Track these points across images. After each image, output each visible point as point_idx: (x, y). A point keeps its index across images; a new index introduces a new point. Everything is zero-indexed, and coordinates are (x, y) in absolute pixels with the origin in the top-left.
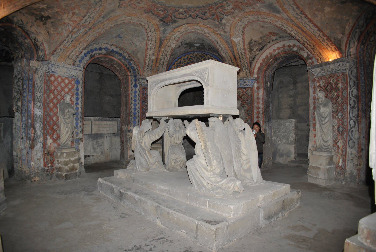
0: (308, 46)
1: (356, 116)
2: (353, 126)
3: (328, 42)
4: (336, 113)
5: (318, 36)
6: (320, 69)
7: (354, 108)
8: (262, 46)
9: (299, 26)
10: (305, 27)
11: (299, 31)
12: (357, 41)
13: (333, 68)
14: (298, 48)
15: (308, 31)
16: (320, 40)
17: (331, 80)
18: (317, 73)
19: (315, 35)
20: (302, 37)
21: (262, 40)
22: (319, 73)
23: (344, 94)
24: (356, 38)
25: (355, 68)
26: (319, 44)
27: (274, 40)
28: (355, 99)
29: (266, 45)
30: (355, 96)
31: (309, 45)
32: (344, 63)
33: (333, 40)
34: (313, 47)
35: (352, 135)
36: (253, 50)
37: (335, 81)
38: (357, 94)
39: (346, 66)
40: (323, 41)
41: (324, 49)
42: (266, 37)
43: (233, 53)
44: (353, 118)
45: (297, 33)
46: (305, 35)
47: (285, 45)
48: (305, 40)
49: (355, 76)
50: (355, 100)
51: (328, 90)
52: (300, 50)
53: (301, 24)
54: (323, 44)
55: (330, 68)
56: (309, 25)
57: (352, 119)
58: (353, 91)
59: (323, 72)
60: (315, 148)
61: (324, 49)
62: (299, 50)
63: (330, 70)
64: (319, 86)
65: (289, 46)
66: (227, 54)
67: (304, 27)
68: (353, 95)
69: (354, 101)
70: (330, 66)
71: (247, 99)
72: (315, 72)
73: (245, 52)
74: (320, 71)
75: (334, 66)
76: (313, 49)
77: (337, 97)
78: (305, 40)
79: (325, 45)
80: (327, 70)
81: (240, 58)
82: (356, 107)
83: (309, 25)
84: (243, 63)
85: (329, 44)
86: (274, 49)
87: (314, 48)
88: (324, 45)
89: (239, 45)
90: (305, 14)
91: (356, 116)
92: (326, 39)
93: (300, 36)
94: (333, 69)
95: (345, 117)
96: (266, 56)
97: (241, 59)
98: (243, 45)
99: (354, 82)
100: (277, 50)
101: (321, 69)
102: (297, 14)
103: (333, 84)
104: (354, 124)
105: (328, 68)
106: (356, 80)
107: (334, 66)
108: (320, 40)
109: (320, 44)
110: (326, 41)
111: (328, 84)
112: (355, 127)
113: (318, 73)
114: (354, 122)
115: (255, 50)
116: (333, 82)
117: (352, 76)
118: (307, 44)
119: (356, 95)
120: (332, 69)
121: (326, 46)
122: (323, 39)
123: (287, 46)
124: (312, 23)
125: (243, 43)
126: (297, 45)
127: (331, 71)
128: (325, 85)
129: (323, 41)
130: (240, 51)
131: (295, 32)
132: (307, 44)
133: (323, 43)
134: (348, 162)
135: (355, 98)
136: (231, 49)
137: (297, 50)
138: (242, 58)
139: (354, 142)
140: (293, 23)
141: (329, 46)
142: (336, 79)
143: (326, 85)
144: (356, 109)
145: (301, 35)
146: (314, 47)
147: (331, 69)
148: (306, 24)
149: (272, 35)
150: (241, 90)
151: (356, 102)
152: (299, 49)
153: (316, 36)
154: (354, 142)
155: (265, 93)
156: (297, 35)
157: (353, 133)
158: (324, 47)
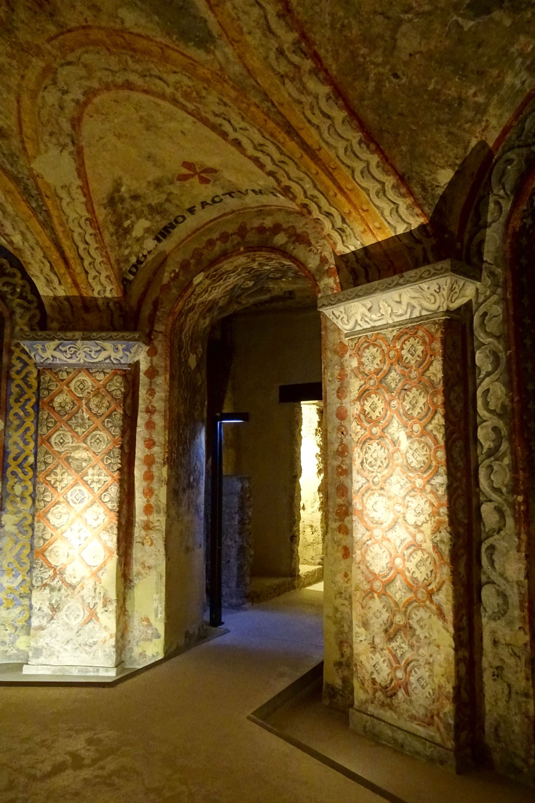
0: (321, 217)
1: (504, 490)
2: (496, 526)
3: (400, 202)
4: (425, 476)
5: (362, 172)
6: (364, 305)
7: (499, 454)
8: (165, 223)
9: (290, 126)
10: (313, 125)
11: (292, 146)
12: (512, 198)
13: (413, 302)
14: (290, 237)
15: (323, 145)
16: (366, 190)
17: (402, 349)
18: (352, 323)
19: (349, 167)
20: (302, 175)
21: (164, 197)
22: (359, 322)
23: (454, 403)
24: (508, 187)
25: (496, 303)
26: (365, 208)
27: (207, 204)
28: (501, 423)
29: (180, 219)
30: (498, 411)
31: (328, 215)
32: (456, 281)
33: (417, 190)
34: (339, 223)
35: (492, 563)
36: (128, 231)
37: (419, 352)
38: (507, 402)
39: (464, 296)
40: (381, 194)
41: (379, 228)
42: (178, 183)
43: (53, 236)
44: (494, 496)
45: (283, 158)
46: (314, 168)
47: (248, 227)
48: (312, 192)
49: (498, 334)
50: (500, 424)
51: (393, 386)
52: (297, 244)
53: (297, 108)
54: (378, 207)
55: (400, 302)
56: (329, 117)
57: (490, 501)
58: (488, 390)
59: (374, 317)
60: (346, 599)
61: (379, 228)
62: (294, 242)
63: (400, 312)
64: (358, 368)
65: (261, 230)
66: (29, 236)
67: (308, 125)
68: (492, 408)
69: (495, 429)
70: (400, 296)
71: (107, 412)
72: (345, 320)
73: (95, 235)
74: (363, 315)
75: (417, 295)
76: (341, 231)
77: (426, 415)
78: (312, 192)
79: (387, 213)
80: (389, 309)
81: (82, 259)
82: (504, 455)
83: (329, 117)
84: (94, 278)
85: (402, 210)
86: (209, 237)
87: (345, 226)
88: (382, 214)
89: (68, 199)
90: (316, 57)
91: (504, 490)
92: (393, 187)
93: (294, 172)
94: (414, 307)
95: (459, 491)
96: (184, 260)
97: (86, 263)
98: (86, 204)
99: (495, 354)
100: (219, 243)
101: (369, 306)
102: (281, 52)
103: (413, 362)
104: (499, 522)
105: (393, 304)
106: (501, 347)
107: (417, 295)
108: (366, 190)
109: (367, 211)
110: (391, 194)
111: (392, 364)
112: (502, 533)
113: (356, 321)
114: (499, 510)
115: (138, 232)
116: (413, 356)
117: (486, 332)
118: (319, 207)
119: (503, 406)
120: (408, 304)
121: (390, 219)
122: (379, 186)
123: (252, 229)
124: (341, 108)
125: (85, 195)
126: (285, 226)
127: (406, 312)
128: (381, 366)
129: (381, 194)
130: (77, 230)
131: (277, 156)
132: (319, 207)
133: (377, 202)
134: (314, 404)
135: (500, 416)
136: (41, 218)
137: (287, 243)
138: (90, 260)
139: (502, 595)
140: (266, 105)
141: (400, 217)
142: (424, 343)
143: (386, 368)
144: (506, 461)
145: (298, 168)
146: (343, 221)
147: (404, 307)
148: (317, 112)
149: (196, 180)
150: (87, 378)
151: (505, 432)
152: (293, 239)
153: (353, 172)
154: (502, 595)
155: (176, 391)
156: (283, 165)
157: (495, 557)
158: (381, 223)
